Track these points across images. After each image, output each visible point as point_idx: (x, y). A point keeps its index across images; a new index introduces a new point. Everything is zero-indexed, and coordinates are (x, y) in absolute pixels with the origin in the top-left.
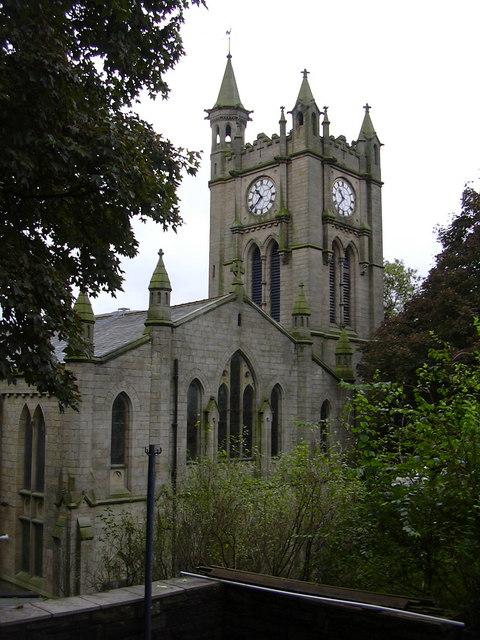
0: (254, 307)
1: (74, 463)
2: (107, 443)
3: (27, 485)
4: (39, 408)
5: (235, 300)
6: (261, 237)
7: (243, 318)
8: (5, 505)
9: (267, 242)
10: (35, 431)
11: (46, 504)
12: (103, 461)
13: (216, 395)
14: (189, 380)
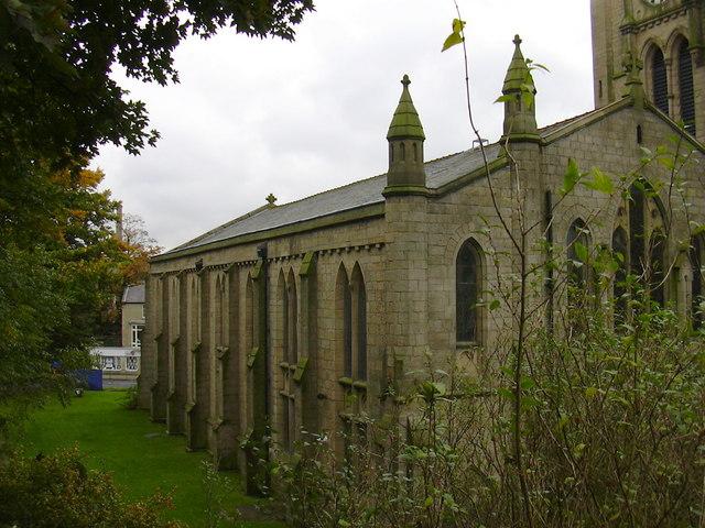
0: (660, 116)
1: (401, 340)
2: (450, 310)
3: (348, 372)
4: (357, 265)
5: (630, 106)
6: (662, 33)
7: (644, 131)
8: (322, 397)
9: (673, 39)
10: (354, 297)
11: (370, 398)
12: (443, 336)
13: (609, 242)
14: (569, 220)
